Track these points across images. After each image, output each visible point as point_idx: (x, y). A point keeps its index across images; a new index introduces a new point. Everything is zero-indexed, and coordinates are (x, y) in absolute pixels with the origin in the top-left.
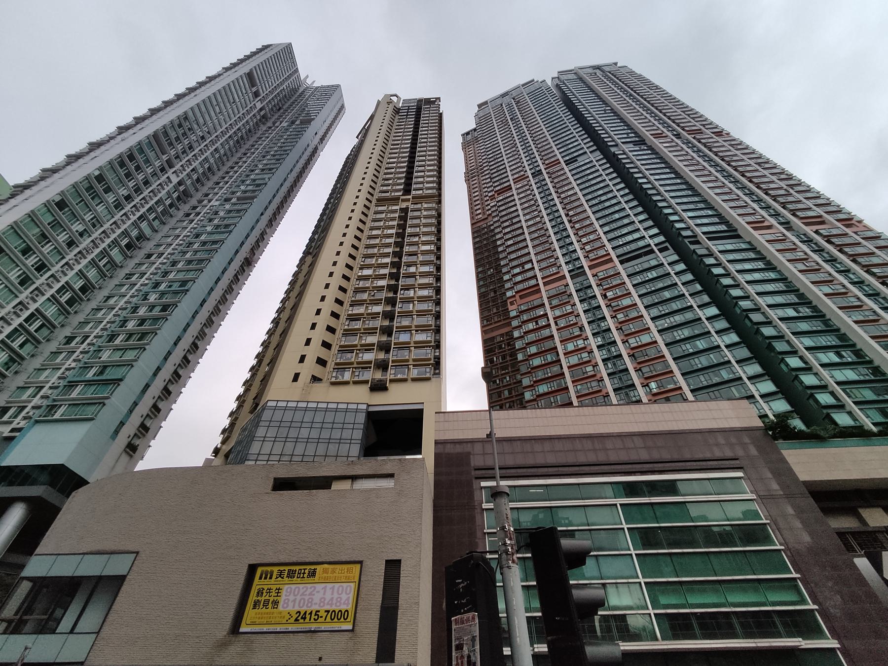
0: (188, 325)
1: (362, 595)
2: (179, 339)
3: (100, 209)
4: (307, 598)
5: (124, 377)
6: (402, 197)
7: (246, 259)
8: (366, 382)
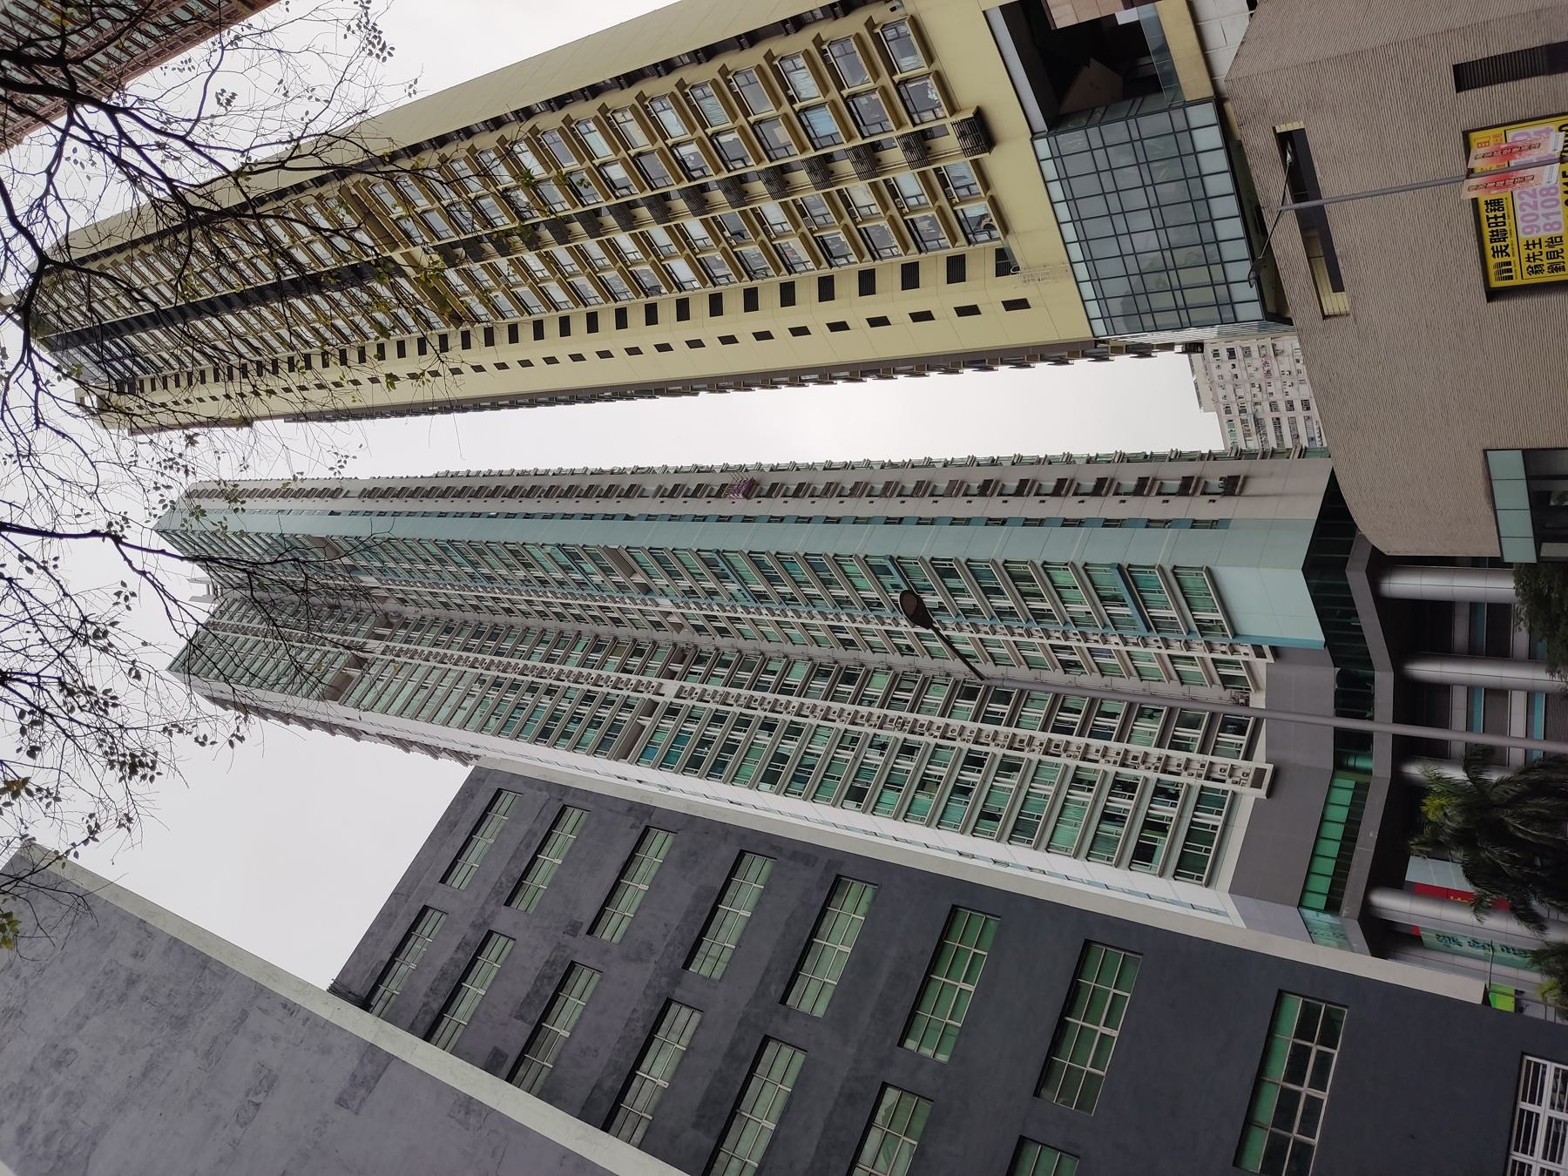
0: (954, 521)
1: (1530, 114)
2: (990, 521)
3: (819, 748)
4: (1540, 199)
5: (1110, 565)
6: (410, 271)
7: (747, 496)
8: (977, 165)
